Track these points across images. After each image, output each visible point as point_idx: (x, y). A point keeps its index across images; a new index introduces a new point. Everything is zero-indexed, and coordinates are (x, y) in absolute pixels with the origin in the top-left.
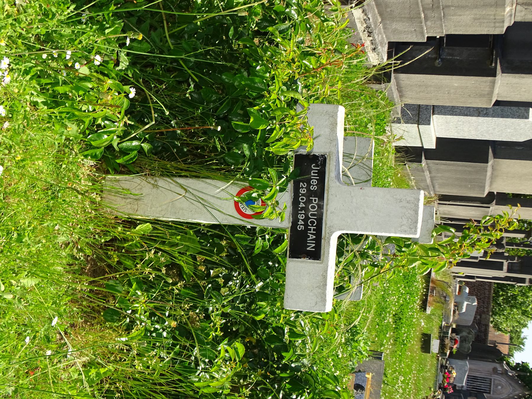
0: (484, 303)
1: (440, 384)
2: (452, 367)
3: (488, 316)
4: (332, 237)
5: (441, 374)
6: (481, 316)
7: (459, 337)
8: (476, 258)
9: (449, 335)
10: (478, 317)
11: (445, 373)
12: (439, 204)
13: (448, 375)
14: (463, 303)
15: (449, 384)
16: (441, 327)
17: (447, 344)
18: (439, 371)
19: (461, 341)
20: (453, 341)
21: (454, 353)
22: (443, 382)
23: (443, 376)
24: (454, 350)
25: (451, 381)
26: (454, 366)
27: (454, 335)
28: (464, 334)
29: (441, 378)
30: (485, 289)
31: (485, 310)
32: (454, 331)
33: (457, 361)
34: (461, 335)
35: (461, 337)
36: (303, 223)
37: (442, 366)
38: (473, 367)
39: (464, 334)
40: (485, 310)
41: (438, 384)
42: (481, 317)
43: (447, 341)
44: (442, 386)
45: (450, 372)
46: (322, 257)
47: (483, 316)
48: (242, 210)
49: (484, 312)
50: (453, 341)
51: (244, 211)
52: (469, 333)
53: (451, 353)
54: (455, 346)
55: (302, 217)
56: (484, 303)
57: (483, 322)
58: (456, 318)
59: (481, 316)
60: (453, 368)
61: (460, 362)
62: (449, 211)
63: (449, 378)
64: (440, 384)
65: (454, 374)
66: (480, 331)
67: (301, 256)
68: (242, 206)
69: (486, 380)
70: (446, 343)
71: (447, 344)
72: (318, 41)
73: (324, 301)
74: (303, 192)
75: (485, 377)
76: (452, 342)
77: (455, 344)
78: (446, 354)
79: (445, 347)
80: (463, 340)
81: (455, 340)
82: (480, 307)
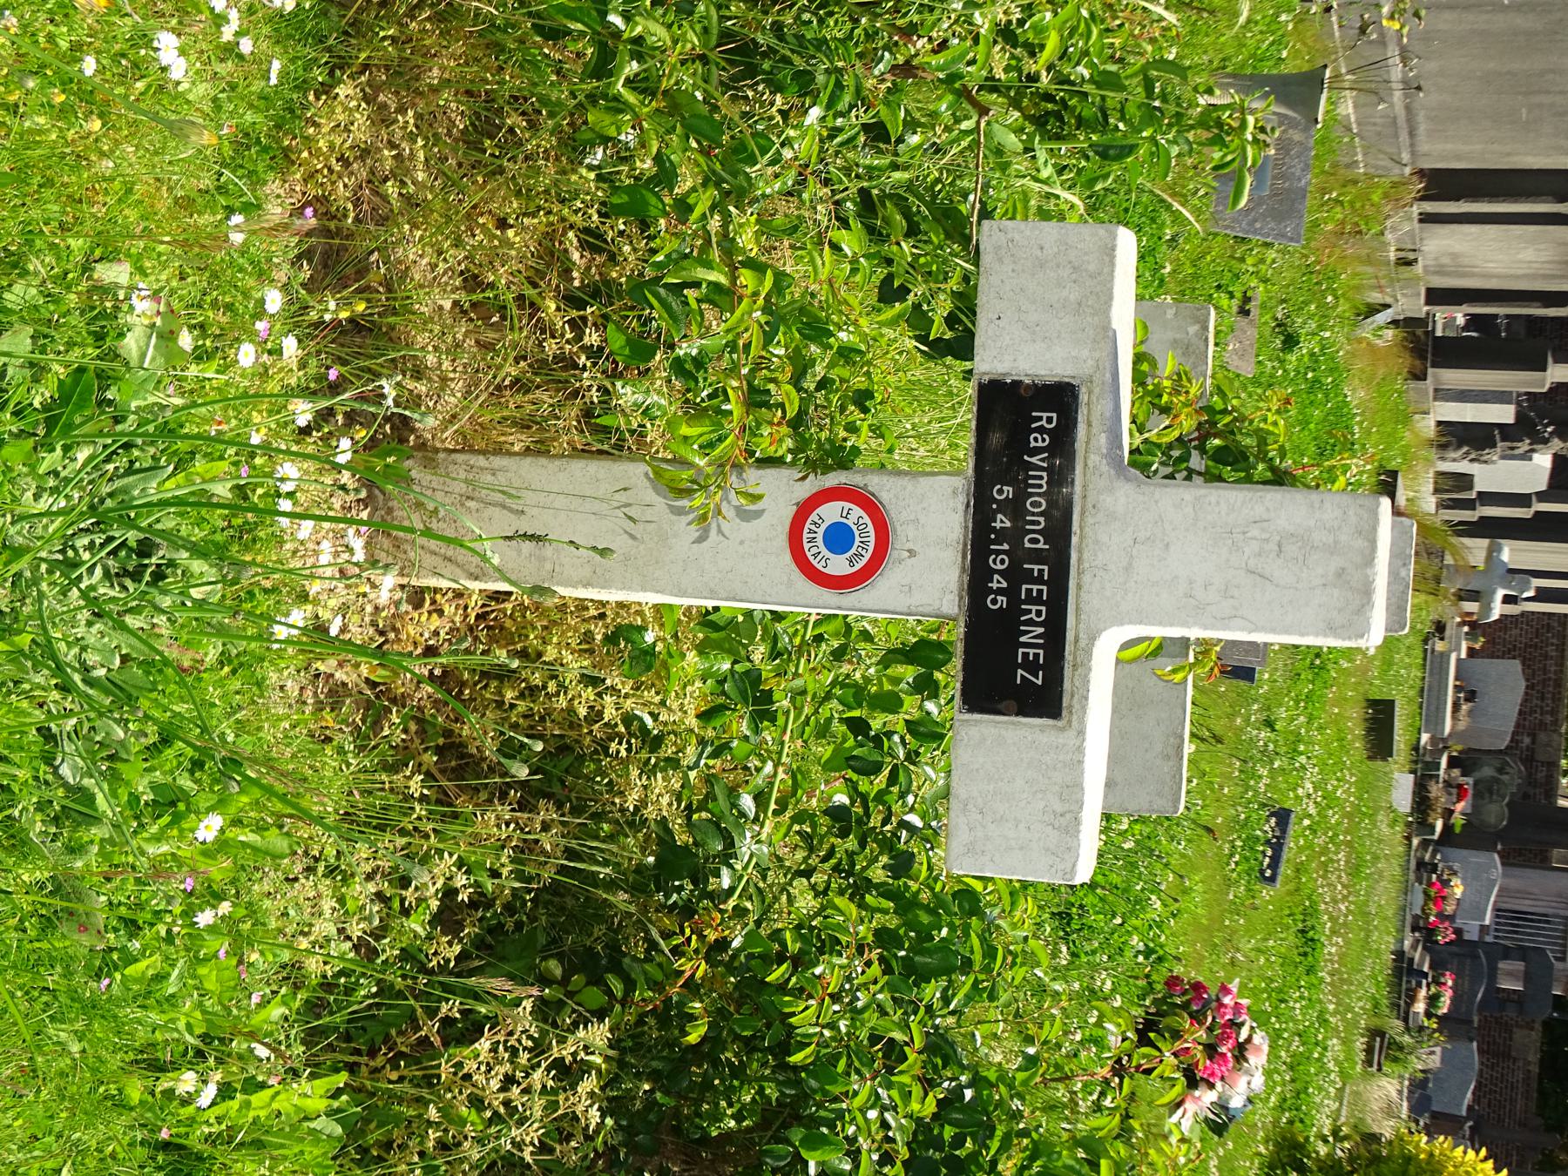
0: (1543, 699)
1: (1416, 917)
2: (1450, 868)
3: (1555, 736)
4: (1096, 651)
5: (1419, 888)
6: (1533, 736)
7: (1470, 780)
8: (1522, 500)
9: (1442, 772)
10: (1527, 740)
11: (1430, 884)
12: (1426, 218)
13: (1440, 890)
14: (1494, 592)
15: (1442, 916)
16: (1416, 748)
17: (1437, 799)
18: (1412, 876)
19: (1478, 795)
20: (1454, 791)
21: (1458, 830)
22: (1423, 910)
23: (1426, 893)
24: (1458, 820)
25: (1449, 909)
26: (1456, 866)
27: (1456, 772)
28: (1487, 772)
29: (1419, 899)
30: (1546, 657)
31: (1548, 718)
32: (1453, 762)
33: (1465, 852)
34: (1477, 775)
35: (1475, 784)
36: (1005, 585)
37: (1421, 864)
38: (1514, 883)
39: (1487, 772)
40: (1548, 718)
41: (1408, 917)
42: (1533, 742)
43: (1435, 790)
44: (1421, 923)
45: (1446, 883)
46: (1064, 713)
47: (1542, 737)
48: (814, 563)
49: (1542, 725)
50: (1454, 791)
51: (819, 567)
52: (1501, 770)
53: (1447, 828)
54: (1460, 806)
55: (1002, 562)
56: (1543, 699)
57: (1541, 756)
58: (1462, 726)
59: (1533, 736)
60: (1455, 873)
61: (1477, 858)
62: (1454, 256)
63: (1444, 898)
64: (1416, 917)
65: (1458, 891)
66: (1530, 781)
67: (1001, 706)
68: (814, 550)
69: (1548, 922)
70: (1432, 795)
71: (1437, 799)
72: (167, 239)
73: (1073, 851)
74: (999, 567)
75: (1550, 911)
76: (1450, 794)
77: (1459, 801)
78: (1433, 827)
79: (1429, 807)
80: (1484, 791)
81: (1460, 786)
82: (1532, 712)
